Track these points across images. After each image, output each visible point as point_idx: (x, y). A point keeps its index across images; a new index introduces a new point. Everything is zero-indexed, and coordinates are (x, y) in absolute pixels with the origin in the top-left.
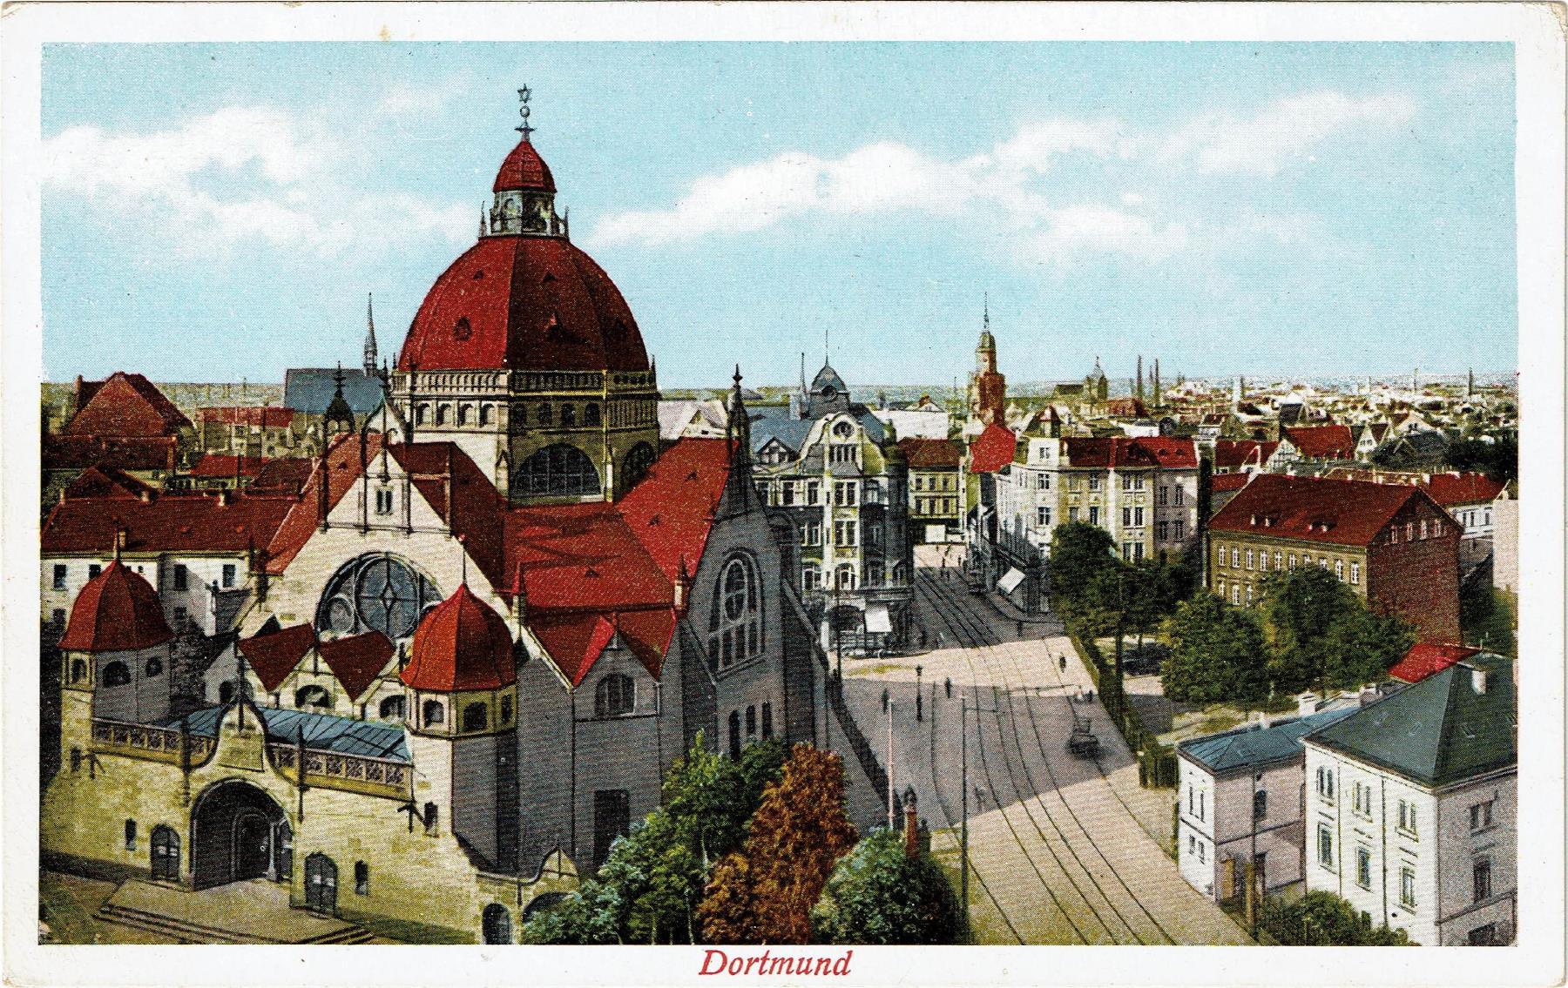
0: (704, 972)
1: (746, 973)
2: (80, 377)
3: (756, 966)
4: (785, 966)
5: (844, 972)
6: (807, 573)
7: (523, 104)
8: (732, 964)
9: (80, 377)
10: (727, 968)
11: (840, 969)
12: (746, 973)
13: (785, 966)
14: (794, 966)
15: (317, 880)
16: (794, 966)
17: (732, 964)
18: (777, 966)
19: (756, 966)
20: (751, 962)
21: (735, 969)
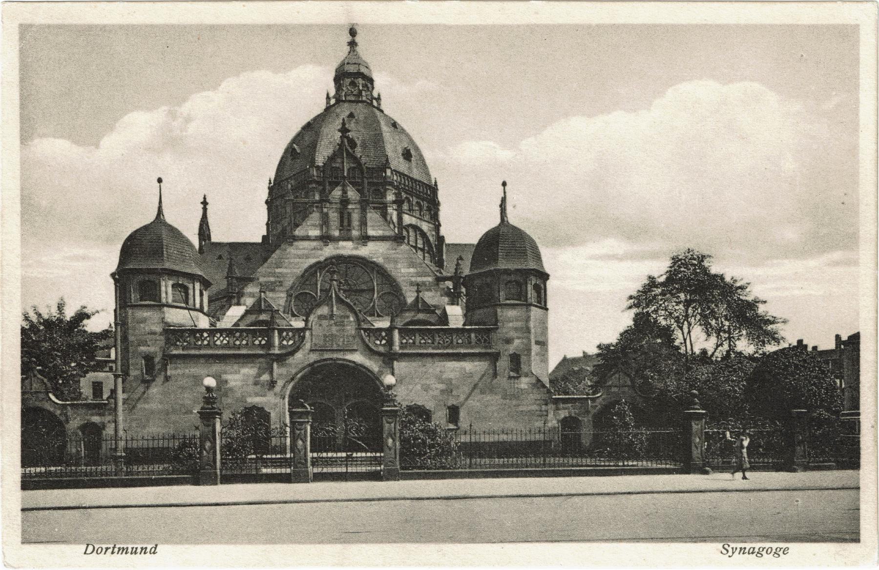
0: (85, 553)
1: (105, 553)
2: (838, 337)
3: (110, 551)
4: (125, 551)
5: (154, 553)
6: (313, 465)
7: (755, 554)
8: (98, 550)
9: (838, 337)
10: (95, 551)
11: (751, 552)
12: (105, 553)
13: (125, 551)
14: (747, 550)
15: (404, 341)
16: (747, 550)
17: (98, 550)
18: (121, 551)
19: (110, 551)
20: (107, 549)
21: (99, 551)
